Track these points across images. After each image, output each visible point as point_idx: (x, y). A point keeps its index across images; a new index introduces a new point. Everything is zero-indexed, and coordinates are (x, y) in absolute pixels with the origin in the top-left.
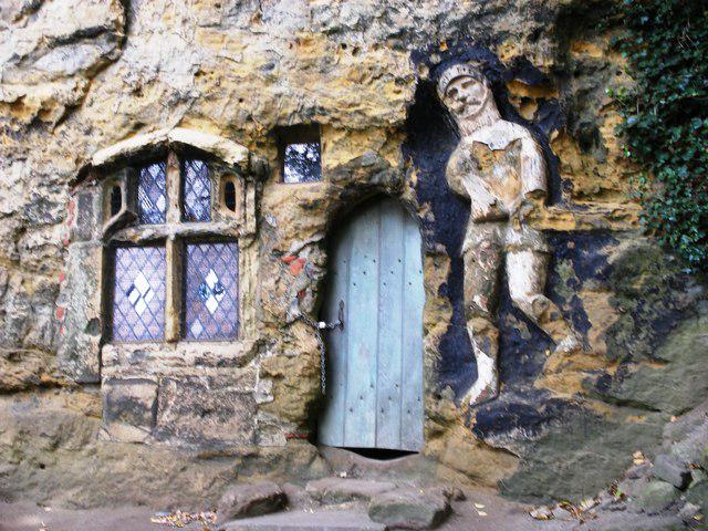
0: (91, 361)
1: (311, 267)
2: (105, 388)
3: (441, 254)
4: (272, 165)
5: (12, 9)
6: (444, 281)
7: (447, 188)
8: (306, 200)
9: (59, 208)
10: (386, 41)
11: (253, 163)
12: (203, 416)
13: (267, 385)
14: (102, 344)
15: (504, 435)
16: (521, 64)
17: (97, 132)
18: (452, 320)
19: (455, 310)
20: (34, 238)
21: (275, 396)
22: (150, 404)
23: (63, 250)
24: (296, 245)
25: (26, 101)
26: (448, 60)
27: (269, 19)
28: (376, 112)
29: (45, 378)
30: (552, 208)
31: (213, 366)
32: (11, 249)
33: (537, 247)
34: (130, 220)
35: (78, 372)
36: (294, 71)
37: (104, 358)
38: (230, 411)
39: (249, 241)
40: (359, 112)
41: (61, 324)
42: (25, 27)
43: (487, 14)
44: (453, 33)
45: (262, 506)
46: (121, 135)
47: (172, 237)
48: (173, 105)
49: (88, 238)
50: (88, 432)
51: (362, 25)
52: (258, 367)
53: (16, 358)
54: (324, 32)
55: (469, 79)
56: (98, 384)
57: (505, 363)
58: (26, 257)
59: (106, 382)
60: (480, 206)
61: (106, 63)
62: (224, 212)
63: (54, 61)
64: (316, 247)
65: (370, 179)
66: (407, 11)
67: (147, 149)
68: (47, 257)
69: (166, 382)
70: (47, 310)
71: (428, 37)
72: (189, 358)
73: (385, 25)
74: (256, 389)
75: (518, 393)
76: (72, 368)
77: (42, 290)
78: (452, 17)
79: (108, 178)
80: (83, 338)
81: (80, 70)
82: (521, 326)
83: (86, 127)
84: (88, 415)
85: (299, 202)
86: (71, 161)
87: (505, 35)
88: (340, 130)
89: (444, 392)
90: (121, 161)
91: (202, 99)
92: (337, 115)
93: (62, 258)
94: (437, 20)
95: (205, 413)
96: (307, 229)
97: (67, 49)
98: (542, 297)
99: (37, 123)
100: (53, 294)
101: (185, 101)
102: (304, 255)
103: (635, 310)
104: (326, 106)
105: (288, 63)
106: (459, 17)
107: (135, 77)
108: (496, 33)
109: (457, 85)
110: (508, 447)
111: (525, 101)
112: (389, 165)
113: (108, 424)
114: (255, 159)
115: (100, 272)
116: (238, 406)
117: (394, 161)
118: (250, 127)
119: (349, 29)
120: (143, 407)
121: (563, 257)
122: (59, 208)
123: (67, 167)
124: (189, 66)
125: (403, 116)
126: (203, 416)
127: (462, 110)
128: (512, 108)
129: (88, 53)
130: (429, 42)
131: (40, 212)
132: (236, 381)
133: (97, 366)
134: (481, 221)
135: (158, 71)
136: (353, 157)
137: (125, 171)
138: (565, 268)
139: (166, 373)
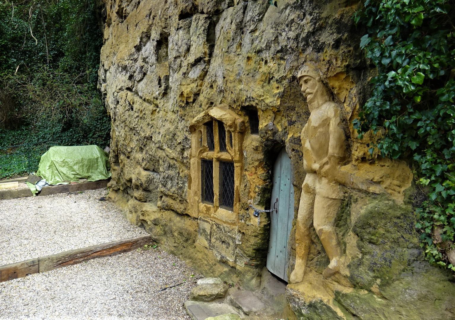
10: (276, 55)
12: (222, 243)
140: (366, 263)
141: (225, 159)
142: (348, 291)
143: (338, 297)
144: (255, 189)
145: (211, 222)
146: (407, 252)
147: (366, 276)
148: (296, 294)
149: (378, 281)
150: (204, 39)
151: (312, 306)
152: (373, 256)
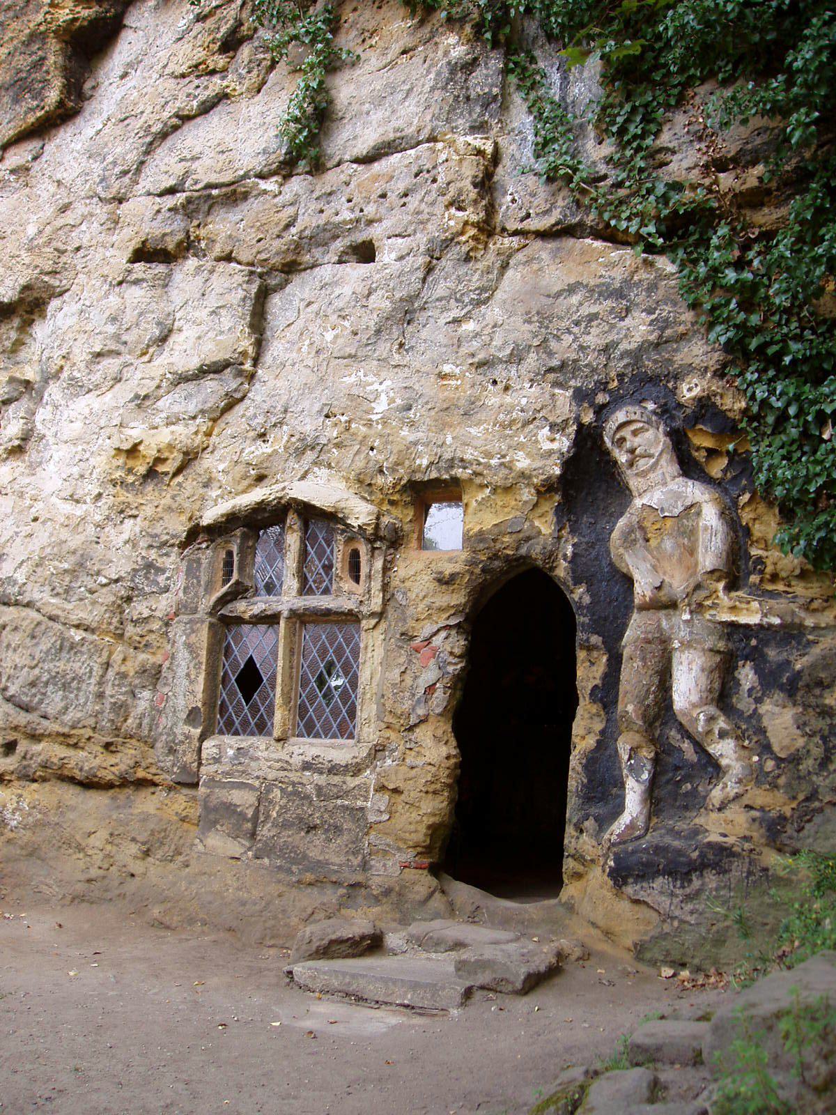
0: (190, 758)
1: (445, 656)
2: (202, 790)
3: (595, 647)
4: (406, 528)
5: (138, 342)
6: (598, 682)
7: (611, 564)
8: (441, 573)
9: (167, 574)
11: (382, 526)
13: (383, 801)
14: (202, 738)
15: (644, 884)
16: (705, 406)
17: (215, 485)
18: (602, 732)
19: (608, 721)
20: (140, 608)
21: (390, 813)
22: (250, 813)
23: (167, 624)
24: (427, 629)
25: (141, 448)
26: (618, 400)
27: (412, 348)
28: (523, 462)
29: (141, 774)
30: (734, 594)
31: (321, 773)
32: (115, 620)
33: (708, 645)
34: (238, 592)
35: (175, 769)
36: (433, 412)
37: (204, 755)
38: (338, 830)
39: (373, 622)
41: (160, 712)
42: (149, 362)
43: (666, 342)
44: (625, 366)
45: (343, 947)
46: (240, 488)
47: (285, 614)
48: (300, 453)
49: (195, 611)
50: (182, 841)
51: (516, 357)
52: (373, 776)
53: (113, 748)
54: (471, 364)
55: (640, 425)
56: (195, 785)
57: (661, 793)
58: (130, 630)
59: (205, 784)
60: (643, 588)
61: (232, 403)
62: (348, 585)
63: (170, 403)
64: (453, 632)
65: (517, 549)
66: (571, 338)
67: (261, 507)
68: (151, 631)
69: (269, 790)
70: (146, 694)
71: (594, 370)
72: (297, 761)
73: (544, 356)
74: (369, 804)
75: (671, 831)
76: (169, 764)
77: (143, 671)
78: (624, 346)
79: (219, 540)
80: (182, 729)
81: (203, 412)
82: (686, 746)
84: (183, 820)
85: (434, 575)
86: (184, 518)
87: (690, 369)
88: (482, 486)
89: (587, 824)
90: (231, 521)
92: (479, 469)
93: (166, 633)
94: (606, 349)
95: (312, 828)
96: (441, 610)
97: (190, 387)
98: (712, 710)
100: (154, 676)
102: (438, 641)
103: (826, 733)
104: (467, 457)
105: (427, 403)
106: (633, 346)
107: (260, 420)
108: (676, 366)
109: (626, 433)
110: (648, 900)
111: (712, 453)
112: (539, 533)
113: (203, 833)
114: (386, 520)
115: (205, 653)
117: (545, 526)
118: (380, 480)
119: (501, 361)
120: (242, 815)
121: (746, 658)
122: (167, 574)
123: (180, 527)
124: (317, 407)
125: (558, 471)
126: (308, 832)
127: (631, 464)
128: (696, 463)
129: (213, 390)
130: (596, 377)
131: (147, 578)
132: (347, 793)
133: (195, 764)
134: (644, 608)
135: (286, 411)
137: (238, 532)
138: (747, 676)
139: (270, 777)
150: (244, 319)
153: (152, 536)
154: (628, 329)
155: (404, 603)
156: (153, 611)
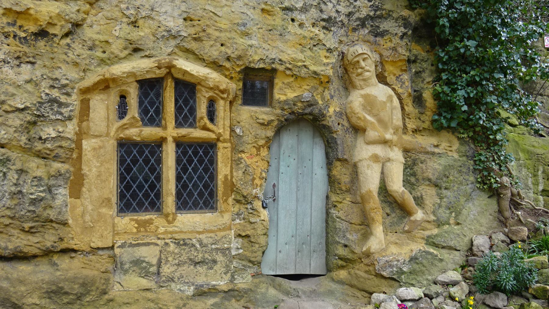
36: (261, 30)
38: (215, 262)
40: (305, 66)
46: (122, 55)
51: (304, 9)
78: (357, 15)
83: (89, 43)
91: (190, 39)
92: (290, 66)
99: (42, 34)
101: (175, 37)
104: (284, 59)
106: (362, 16)
108: (381, 30)
116: (220, 258)
119: (296, 9)
136: (296, 95)
140: (443, 204)
141: (206, 139)
142: (435, 231)
143: (430, 241)
144: (261, 174)
145: (159, 242)
146: (467, 188)
147: (443, 213)
148: (393, 258)
149: (453, 214)
151: (413, 259)
152: (448, 198)
153: (52, 79)
154: (359, 7)
155: (241, 134)
156: (60, 132)
